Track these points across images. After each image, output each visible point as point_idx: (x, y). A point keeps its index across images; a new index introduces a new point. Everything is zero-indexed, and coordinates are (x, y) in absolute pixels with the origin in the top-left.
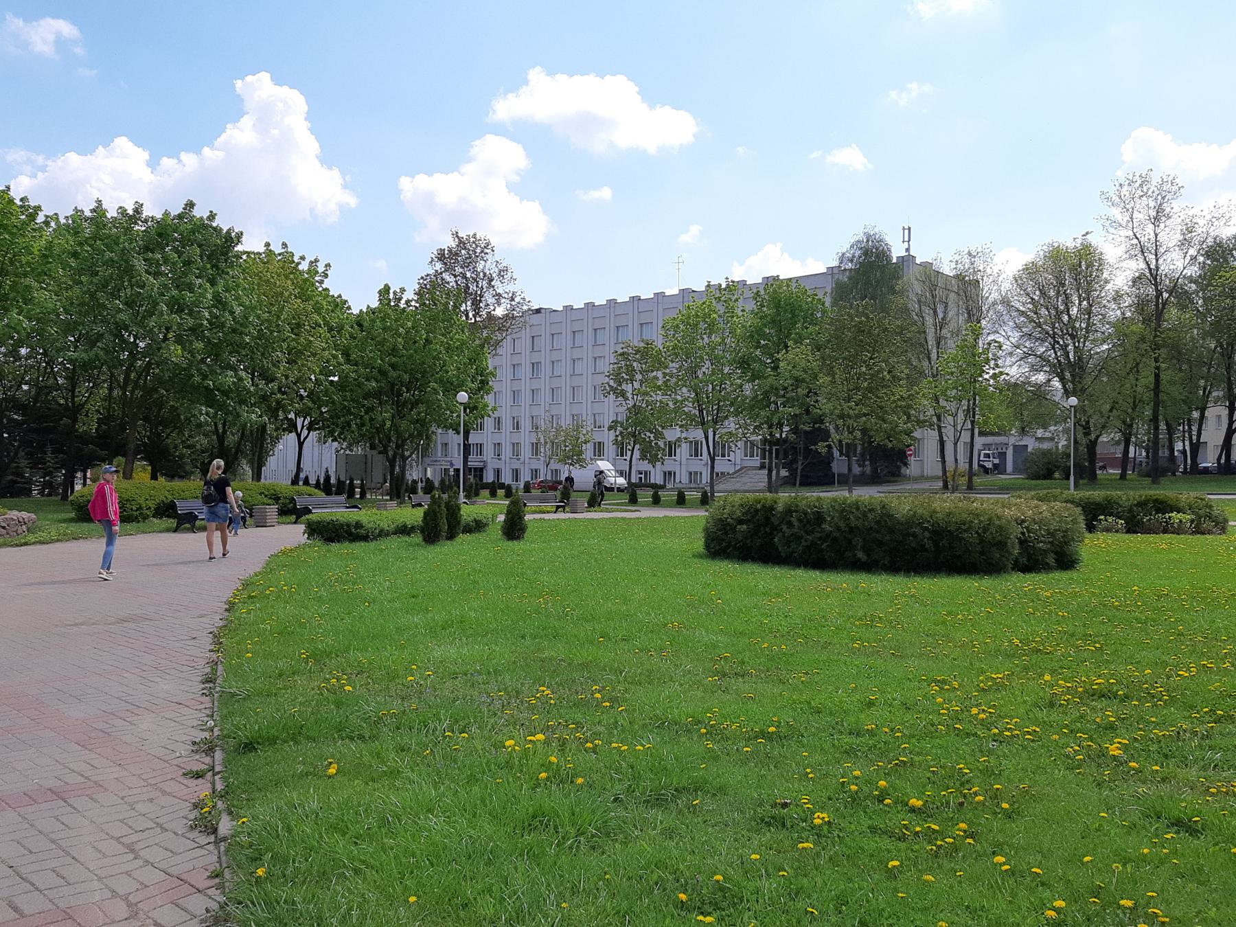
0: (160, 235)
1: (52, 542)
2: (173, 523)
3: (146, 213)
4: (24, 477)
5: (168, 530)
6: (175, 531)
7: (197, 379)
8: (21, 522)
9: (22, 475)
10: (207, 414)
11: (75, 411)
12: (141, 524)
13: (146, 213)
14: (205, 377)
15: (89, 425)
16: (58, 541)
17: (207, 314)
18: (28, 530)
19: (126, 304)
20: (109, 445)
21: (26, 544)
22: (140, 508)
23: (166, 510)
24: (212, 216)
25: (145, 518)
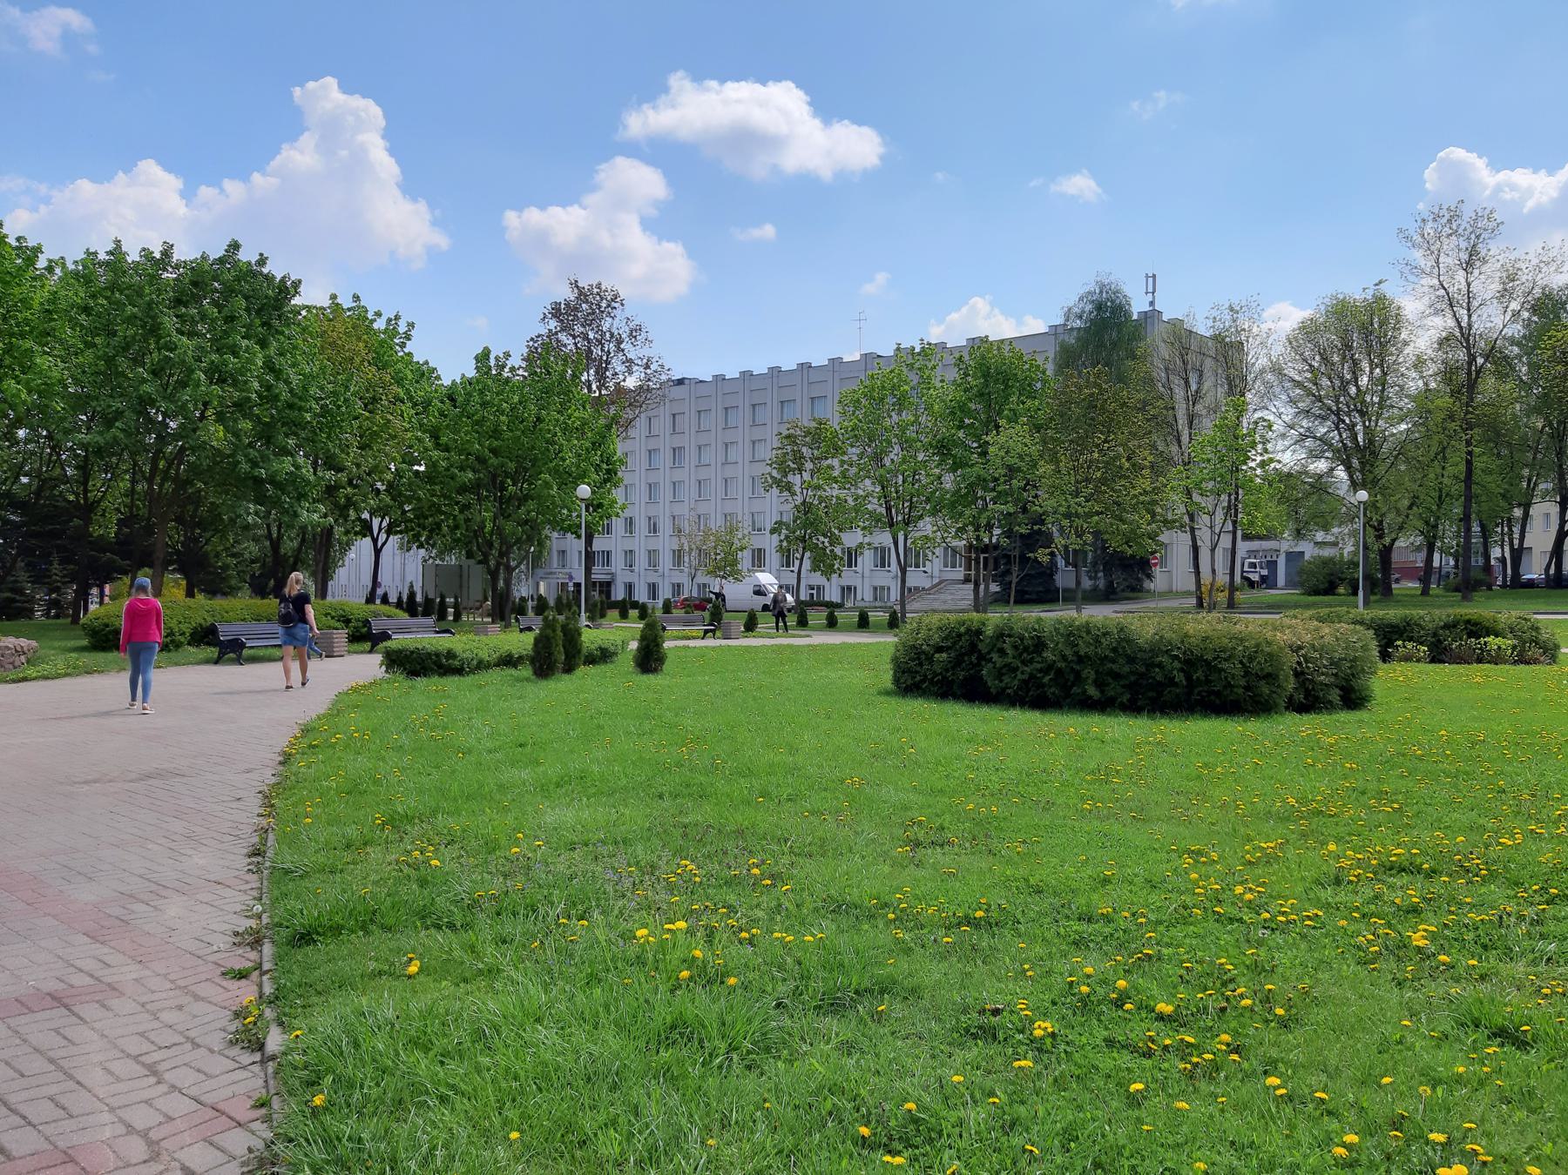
2: (213, 652)
3: (177, 256)
4: (23, 594)
5: (207, 662)
6: (216, 662)
8: (20, 652)
9: (20, 591)
10: (256, 513)
11: (88, 509)
14: (255, 464)
15: (106, 527)
16: (67, 675)
21: (25, 679)
24: (262, 261)
25: (178, 645)
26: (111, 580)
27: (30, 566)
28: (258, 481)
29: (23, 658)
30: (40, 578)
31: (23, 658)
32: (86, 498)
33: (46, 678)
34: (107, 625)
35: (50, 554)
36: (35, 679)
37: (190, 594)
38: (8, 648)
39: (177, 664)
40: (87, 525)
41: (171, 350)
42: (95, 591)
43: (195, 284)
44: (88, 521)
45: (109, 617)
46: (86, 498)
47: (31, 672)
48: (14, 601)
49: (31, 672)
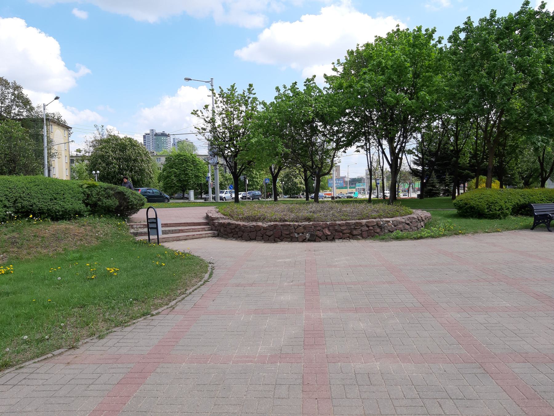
0: (507, 28)
1: (439, 236)
2: (531, 220)
3: (499, 16)
4: (435, 187)
5: (526, 228)
6: (532, 229)
7: (535, 116)
8: (420, 220)
9: (434, 186)
10: (542, 141)
11: (457, 152)
12: (502, 221)
13: (499, 16)
14: (540, 115)
15: (465, 160)
16: (444, 235)
17: (541, 71)
18: (425, 225)
19: (487, 73)
20: (478, 169)
21: (421, 238)
22: (501, 209)
23: (524, 209)
24: (543, 6)
25: (505, 215)
26: (468, 181)
27: (438, 177)
28: (542, 124)
29: (422, 223)
30: (442, 181)
31: (422, 223)
32: (457, 148)
33: (432, 237)
34: (466, 204)
35: (445, 172)
36: (427, 237)
37: (501, 187)
38: (414, 218)
39: (507, 229)
40: (457, 159)
41: (495, 61)
42: (462, 185)
43: (507, 28)
44: (458, 157)
45: (467, 199)
46: (457, 148)
47: (425, 233)
48: (432, 190)
49: (425, 233)
